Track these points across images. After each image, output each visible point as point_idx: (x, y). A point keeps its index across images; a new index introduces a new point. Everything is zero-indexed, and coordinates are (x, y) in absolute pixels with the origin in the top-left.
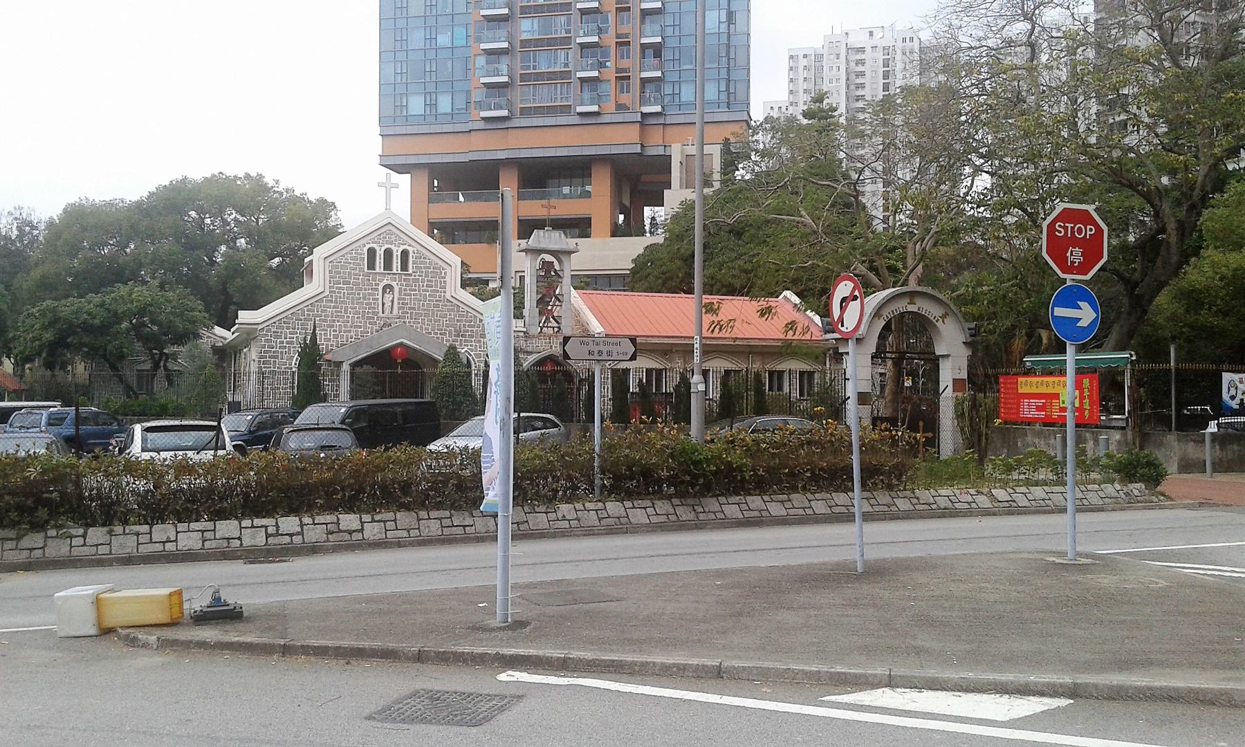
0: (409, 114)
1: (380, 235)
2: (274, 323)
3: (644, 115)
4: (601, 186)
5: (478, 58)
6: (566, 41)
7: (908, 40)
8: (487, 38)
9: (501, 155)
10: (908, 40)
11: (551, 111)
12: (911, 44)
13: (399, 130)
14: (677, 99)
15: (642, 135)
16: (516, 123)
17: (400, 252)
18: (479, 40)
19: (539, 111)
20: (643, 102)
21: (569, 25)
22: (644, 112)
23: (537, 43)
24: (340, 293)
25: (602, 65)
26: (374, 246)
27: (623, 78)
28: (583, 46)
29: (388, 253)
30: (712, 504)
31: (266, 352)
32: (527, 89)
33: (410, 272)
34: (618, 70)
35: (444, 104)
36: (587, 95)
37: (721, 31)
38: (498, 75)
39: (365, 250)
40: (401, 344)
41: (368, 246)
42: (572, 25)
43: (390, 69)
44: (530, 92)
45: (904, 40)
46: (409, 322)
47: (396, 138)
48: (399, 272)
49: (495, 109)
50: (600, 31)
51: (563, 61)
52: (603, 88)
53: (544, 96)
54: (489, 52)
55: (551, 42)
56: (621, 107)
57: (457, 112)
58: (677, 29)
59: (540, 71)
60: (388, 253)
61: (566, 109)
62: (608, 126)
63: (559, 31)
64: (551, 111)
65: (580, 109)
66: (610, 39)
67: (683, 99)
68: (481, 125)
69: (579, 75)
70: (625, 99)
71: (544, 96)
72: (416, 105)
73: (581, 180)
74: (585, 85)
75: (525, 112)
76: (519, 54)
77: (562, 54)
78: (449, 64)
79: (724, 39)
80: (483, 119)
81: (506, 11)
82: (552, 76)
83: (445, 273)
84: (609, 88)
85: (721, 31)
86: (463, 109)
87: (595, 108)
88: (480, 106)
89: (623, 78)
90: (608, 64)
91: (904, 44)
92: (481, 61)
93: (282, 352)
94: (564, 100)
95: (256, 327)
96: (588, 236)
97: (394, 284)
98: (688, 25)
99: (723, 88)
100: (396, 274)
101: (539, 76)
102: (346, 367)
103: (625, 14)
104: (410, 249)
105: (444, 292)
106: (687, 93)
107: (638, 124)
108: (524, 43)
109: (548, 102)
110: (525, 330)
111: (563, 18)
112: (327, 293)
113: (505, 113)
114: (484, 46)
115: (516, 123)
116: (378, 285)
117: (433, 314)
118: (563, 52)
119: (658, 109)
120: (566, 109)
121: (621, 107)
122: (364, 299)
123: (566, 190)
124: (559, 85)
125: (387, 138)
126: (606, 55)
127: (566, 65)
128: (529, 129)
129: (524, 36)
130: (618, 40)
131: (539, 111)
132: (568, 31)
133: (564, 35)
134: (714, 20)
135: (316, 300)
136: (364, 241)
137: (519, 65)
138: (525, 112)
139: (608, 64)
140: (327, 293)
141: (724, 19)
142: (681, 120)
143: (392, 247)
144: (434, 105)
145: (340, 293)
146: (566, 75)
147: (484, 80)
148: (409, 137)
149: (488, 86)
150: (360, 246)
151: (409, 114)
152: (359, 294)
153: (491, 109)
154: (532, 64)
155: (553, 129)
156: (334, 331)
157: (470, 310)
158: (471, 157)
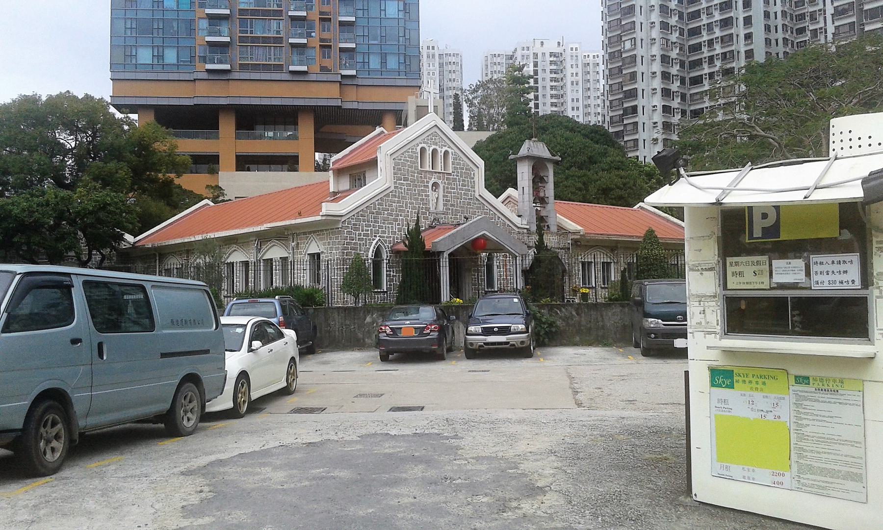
0: (139, 62)
1: (428, 136)
2: (354, 215)
3: (343, 77)
4: (306, 130)
5: (201, 21)
9: (223, 102)
11: (266, 68)
14: (366, 67)
19: (256, 67)
23: (254, 12)
24: (401, 188)
25: (309, 35)
28: (293, 18)
29: (434, 152)
30: (181, 390)
31: (348, 244)
32: (245, 49)
33: (451, 172)
34: (322, 40)
35: (171, 56)
36: (295, 58)
37: (400, 17)
38: (221, 36)
39: (419, 149)
41: (421, 146)
43: (121, 24)
44: (247, 51)
45: (428, 48)
46: (451, 218)
48: (443, 171)
49: (218, 63)
51: (275, 28)
52: (310, 53)
53: (260, 56)
54: (211, 17)
55: (266, 13)
56: (324, 69)
57: (182, 63)
58: (366, 12)
60: (434, 152)
61: (279, 68)
63: (272, 5)
64: (266, 68)
65: (292, 68)
68: (205, 76)
69: (291, 41)
70: (327, 63)
71: (260, 56)
72: (145, 56)
74: (295, 49)
75: (243, 67)
76: (238, 20)
77: (274, 24)
78: (175, 24)
82: (266, 40)
83: (474, 174)
84: (316, 53)
85: (400, 17)
86: (187, 61)
88: (204, 60)
89: (325, 47)
90: (313, 34)
92: (204, 24)
93: (360, 244)
94: (276, 60)
95: (339, 219)
96: (296, 170)
97: (439, 182)
100: (440, 173)
101: (255, 39)
102: (446, 255)
104: (449, 150)
105: (474, 191)
107: (338, 84)
108: (242, 12)
110: (528, 227)
113: (227, 67)
114: (209, 11)
116: (428, 182)
117: (467, 211)
118: (275, 21)
119: (353, 72)
120: (279, 68)
121: (324, 69)
122: (419, 195)
123: (271, 134)
126: (311, 27)
127: (278, 32)
128: (247, 82)
129: (242, 7)
130: (321, 16)
131: (256, 67)
133: (276, 8)
134: (392, 10)
135: (384, 197)
136: (417, 141)
137: (238, 29)
138: (243, 67)
139: (313, 34)
143: (437, 147)
144: (160, 57)
145: (401, 188)
146: (278, 40)
148: (139, 83)
149: (211, 44)
150: (414, 146)
152: (415, 190)
155: (279, 82)
156: (399, 224)
157: (492, 209)
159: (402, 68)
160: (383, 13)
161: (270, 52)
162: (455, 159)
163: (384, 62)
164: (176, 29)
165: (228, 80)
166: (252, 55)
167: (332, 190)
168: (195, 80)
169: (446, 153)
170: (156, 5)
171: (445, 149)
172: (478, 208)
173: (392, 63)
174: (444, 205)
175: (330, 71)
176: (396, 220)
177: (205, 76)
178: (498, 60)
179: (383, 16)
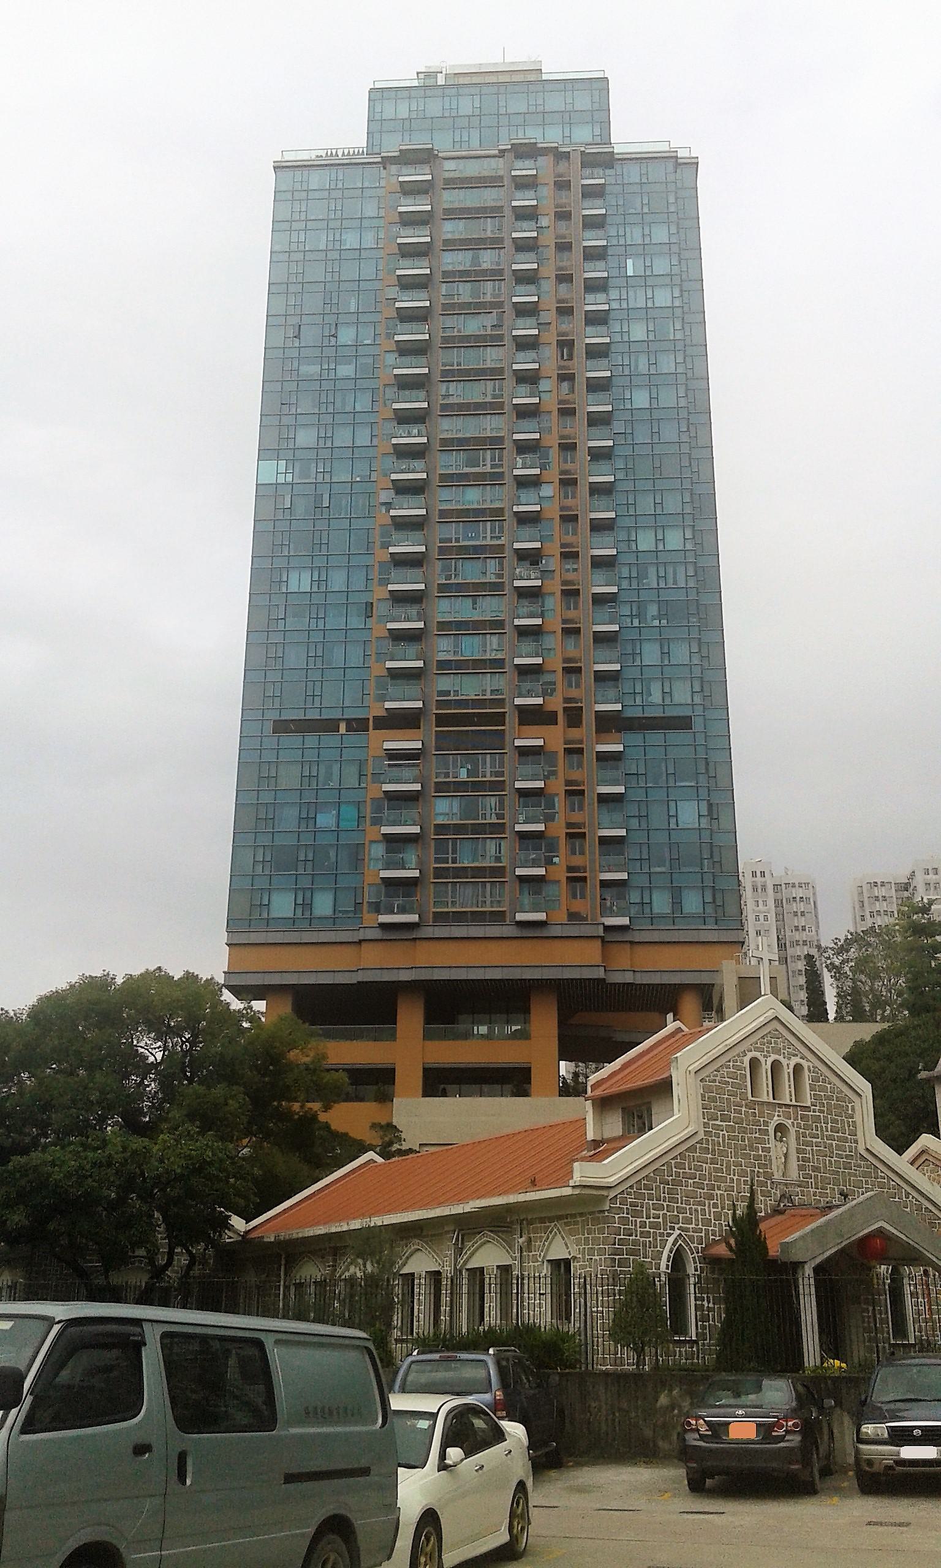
1: (763, 1037)
2: (631, 1187)
3: (608, 929)
6: (499, 828)
7: (758, 874)
8: (388, 820)
9: (405, 976)
10: (758, 874)
11: (478, 917)
12: (763, 879)
13: (254, 938)
14: (647, 910)
15: (604, 957)
16: (428, 932)
17: (791, 1067)
18: (377, 822)
19: (460, 917)
20: (606, 911)
21: (502, 808)
22: (606, 923)
23: (459, 829)
25: (549, 862)
26: (757, 1054)
27: (577, 880)
28: (523, 836)
32: (443, 888)
35: (323, 905)
36: (526, 900)
39: (747, 1060)
40: (880, 1231)
41: (750, 1055)
42: (507, 808)
43: (248, 856)
47: (248, 949)
48: (794, 1103)
50: (543, 467)
52: (549, 890)
53: (465, 900)
54: (389, 839)
59: (463, 865)
61: (498, 917)
62: (557, 941)
64: (478, 917)
65: (520, 917)
66: (559, 830)
67: (656, 910)
68: (377, 934)
70: (578, 906)
71: (465, 900)
72: (283, 905)
73: (522, 1016)
74: (526, 886)
78: (332, 854)
79: (706, 835)
80: (384, 926)
81: (417, 787)
82: (479, 872)
83: (853, 1109)
87: (541, 916)
89: (577, 880)
90: (556, 860)
91: (754, 879)
92: (378, 850)
94: (495, 905)
95: (605, 1193)
96: (526, 1094)
97: (788, 1123)
98: (657, 819)
99: (709, 899)
101: (462, 872)
102: (808, 1270)
103: (575, 757)
105: (856, 1142)
106: (661, 903)
108: (441, 828)
109: (472, 907)
111: (493, 799)
112: (701, 1135)
113: (414, 918)
114: (386, 830)
115: (428, 932)
116: (766, 1124)
119: (625, 921)
120: (498, 917)
121: (574, 916)
122: (752, 1148)
123: (483, 1030)
124: (488, 885)
125: (237, 948)
127: (498, 859)
129: (440, 821)
131: (460, 917)
132: (500, 816)
137: (433, 856)
139: (556, 860)
140: (701, 1135)
141: (704, 812)
142: (656, 937)
143: (781, 1058)
146: (498, 872)
147: (385, 874)
150: (738, 1055)
151: (271, 916)
153: (392, 912)
154: (450, 856)
156: (715, 1206)
158: (361, 977)
159: (710, 910)
160: (673, 821)
161: (484, 892)
162: (815, 1080)
163: (677, 903)
164: (333, 859)
165: (415, 939)
166: (455, 898)
167: (590, 1136)
168: (360, 942)
169: (798, 1069)
170: (322, 442)
171: (795, 1060)
172: (865, 1175)
173: (692, 903)
174: (801, 1168)
175: (586, 919)
176: (711, 1197)
177: (377, 934)
178: (881, 892)
179: (667, 702)
